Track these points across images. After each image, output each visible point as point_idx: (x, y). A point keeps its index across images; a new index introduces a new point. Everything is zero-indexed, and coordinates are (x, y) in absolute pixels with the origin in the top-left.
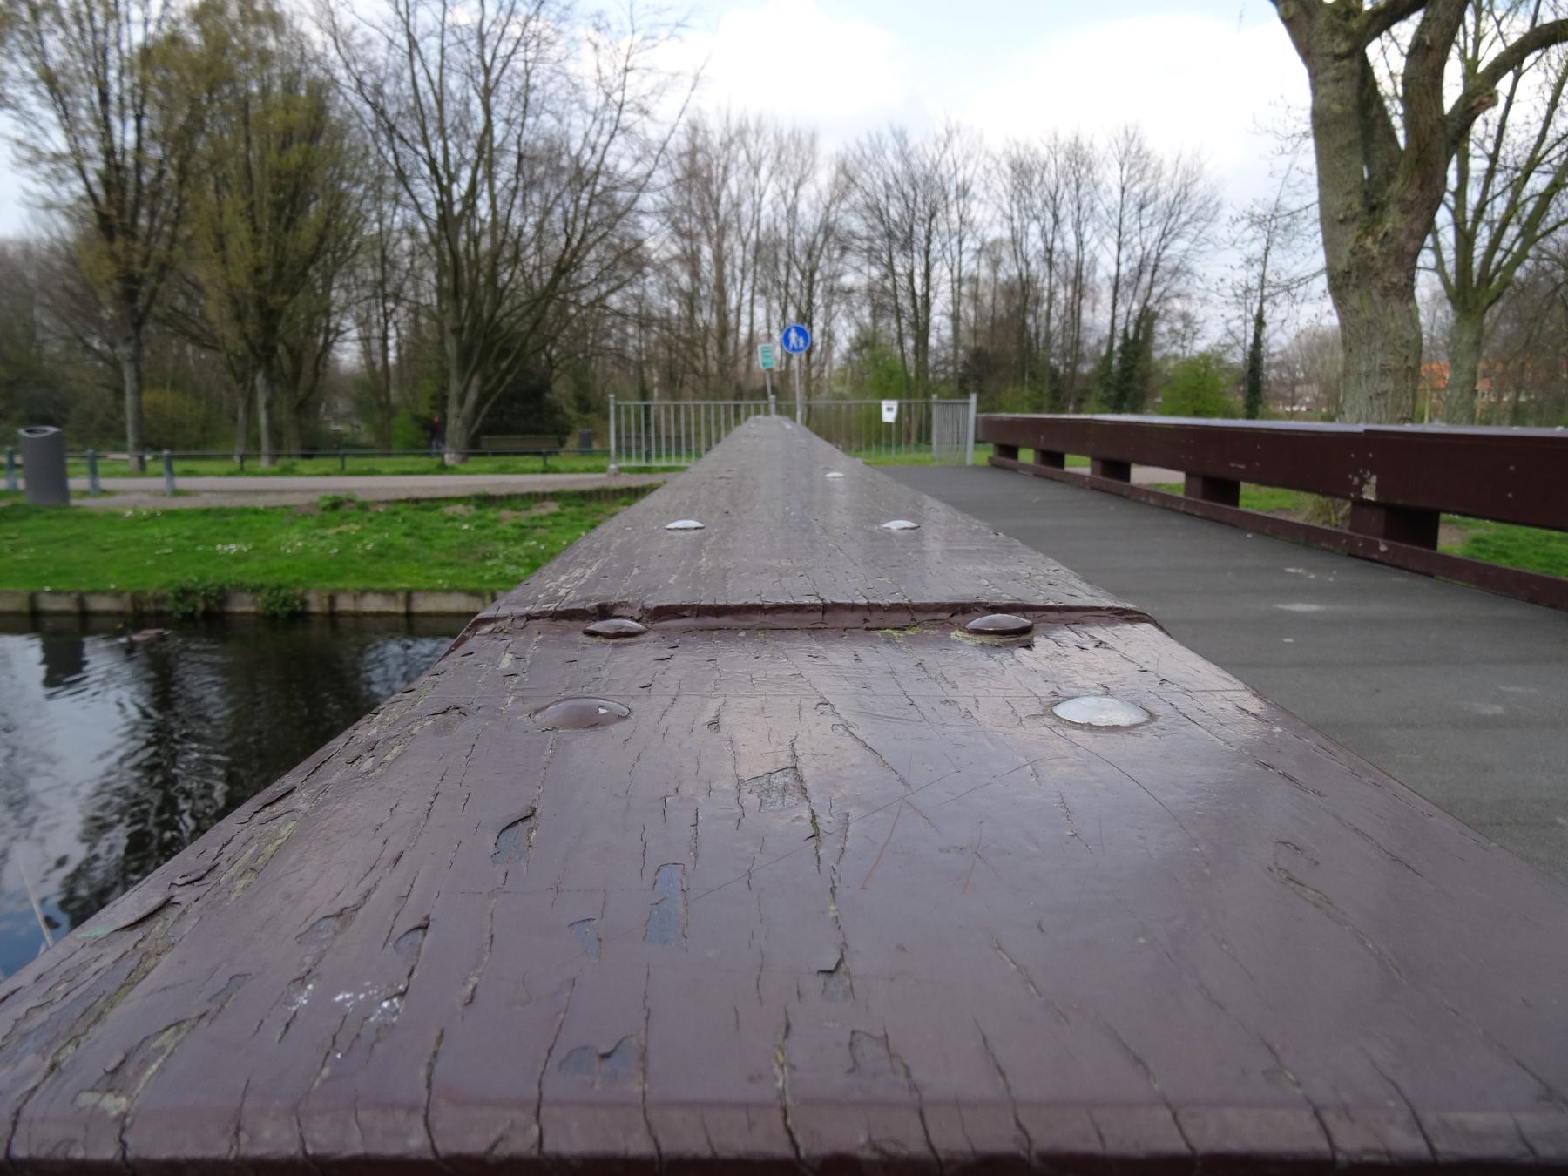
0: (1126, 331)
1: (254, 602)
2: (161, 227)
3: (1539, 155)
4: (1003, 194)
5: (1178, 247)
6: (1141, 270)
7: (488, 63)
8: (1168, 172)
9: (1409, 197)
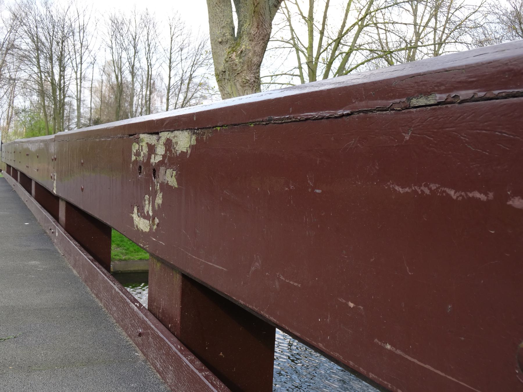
2: (430, 189)
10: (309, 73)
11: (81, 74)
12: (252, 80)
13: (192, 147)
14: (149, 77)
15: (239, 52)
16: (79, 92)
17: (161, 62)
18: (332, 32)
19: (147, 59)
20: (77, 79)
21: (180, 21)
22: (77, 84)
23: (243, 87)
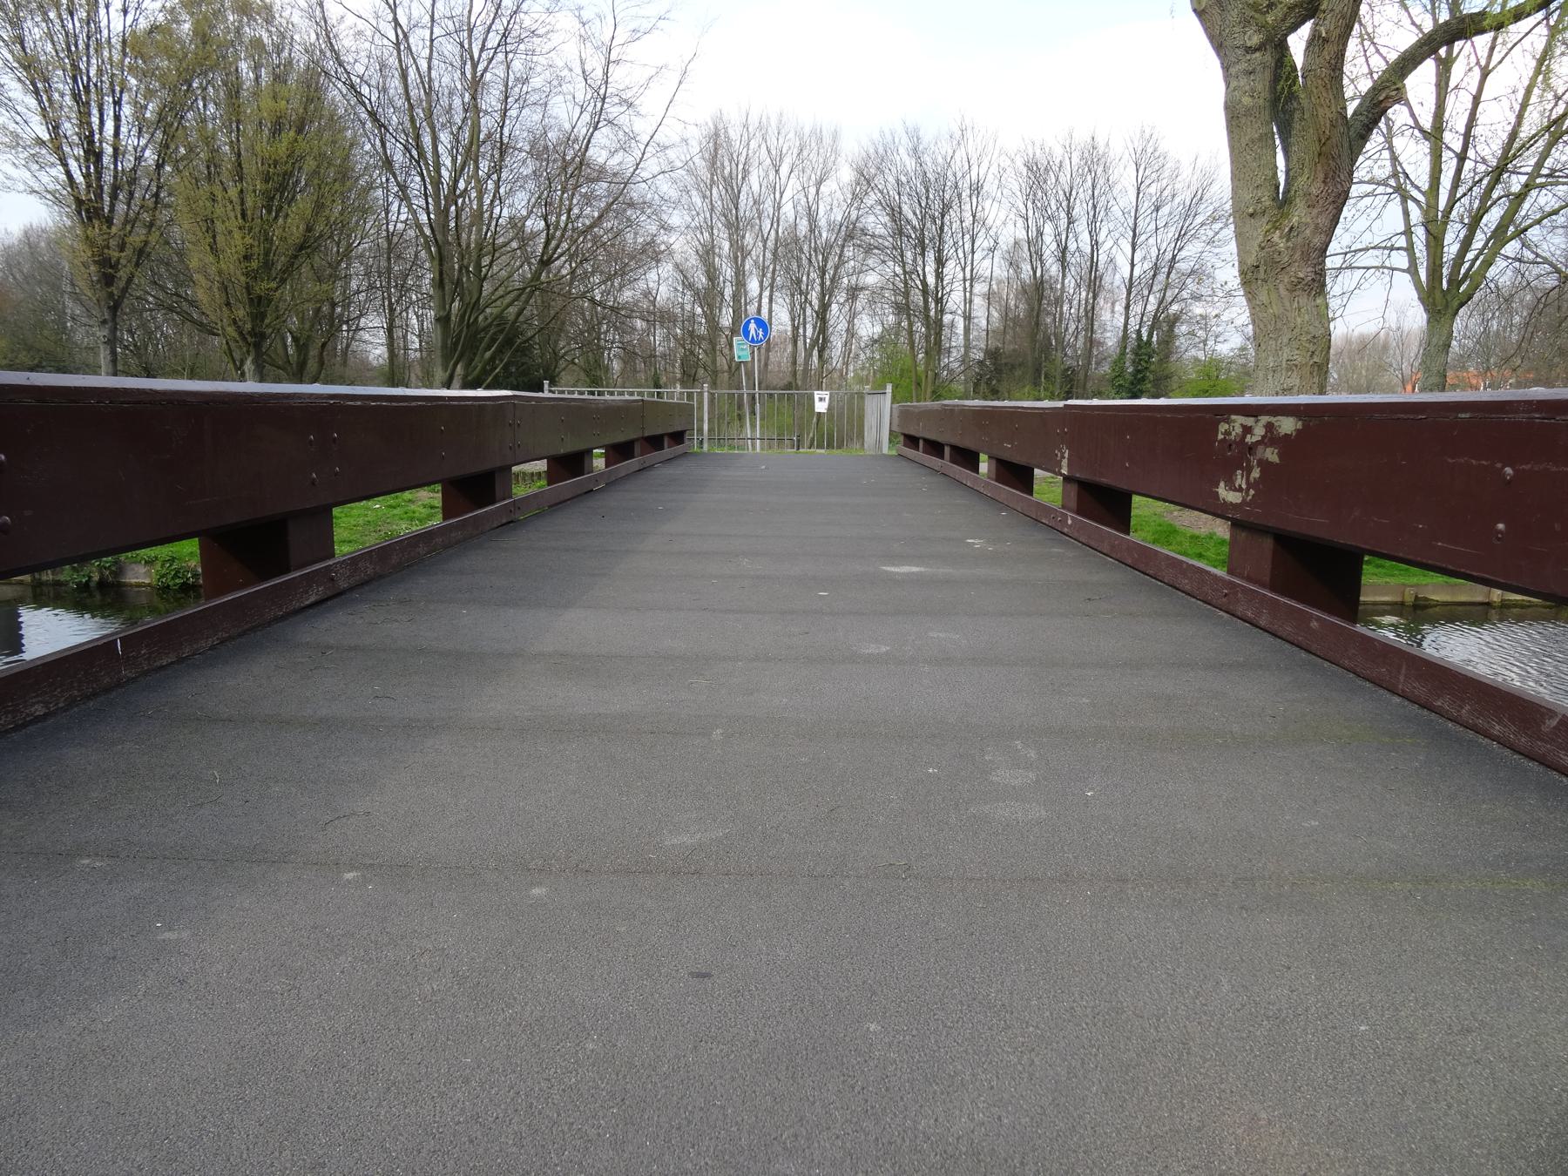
0: (1139, 332)
1: (148, 574)
3: (479, 74)
4: (1019, 193)
5: (1191, 250)
6: (1156, 268)
7: (476, 56)
8: (1186, 172)
9: (1314, 191)
10: (1427, 241)
11: (972, 270)
12: (1310, 278)
13: (1298, 431)
14: (1093, 265)
15: (1287, 230)
16: (969, 302)
17: (1117, 235)
18: (1489, 146)
19: (1090, 233)
20: (965, 280)
21: (1157, 154)
22: (965, 289)
23: (1291, 291)
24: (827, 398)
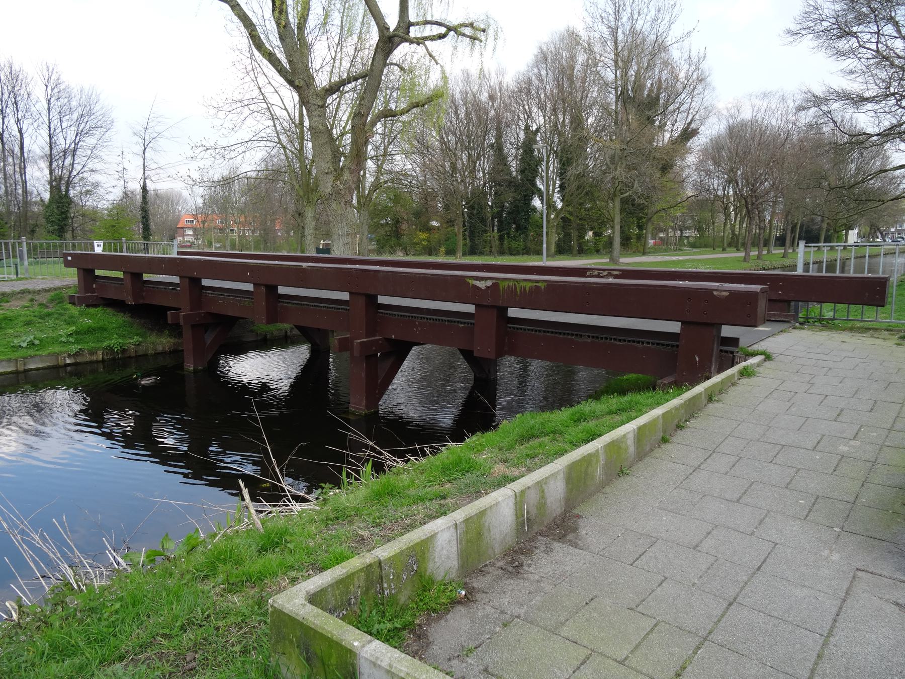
24: (102, 244)
